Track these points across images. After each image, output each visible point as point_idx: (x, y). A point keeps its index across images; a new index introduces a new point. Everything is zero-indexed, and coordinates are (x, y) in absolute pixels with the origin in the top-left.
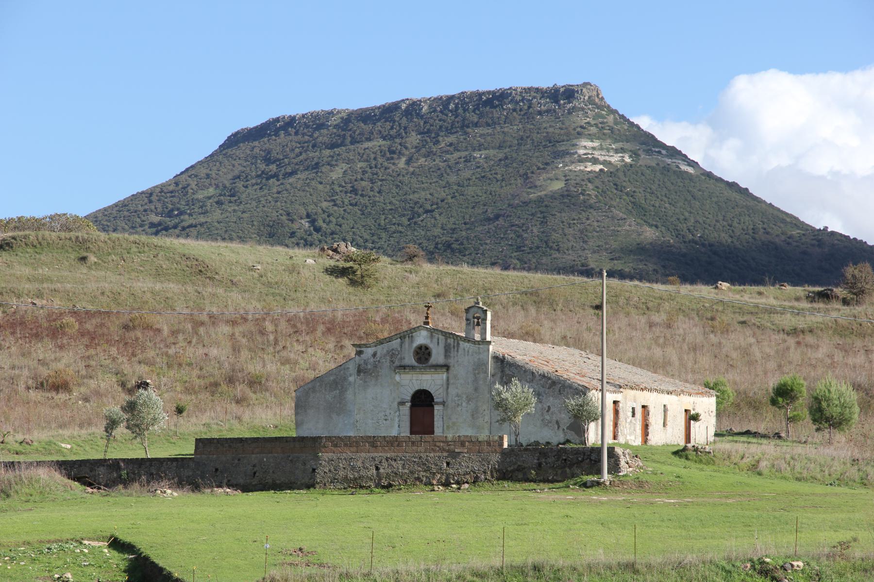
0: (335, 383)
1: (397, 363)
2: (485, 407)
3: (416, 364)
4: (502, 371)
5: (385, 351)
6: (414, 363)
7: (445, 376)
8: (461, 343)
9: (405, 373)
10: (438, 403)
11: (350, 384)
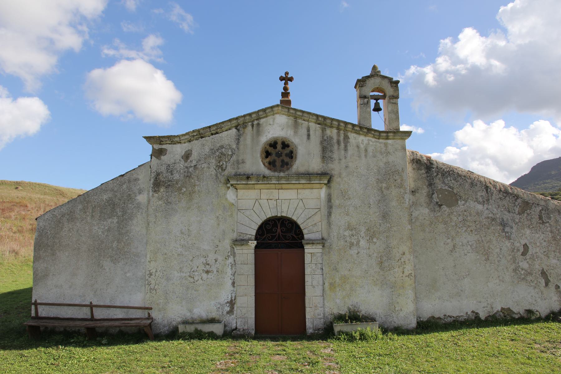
0: (112, 205)
1: (230, 170)
2: (404, 248)
3: (267, 172)
4: (430, 185)
5: (207, 149)
6: (263, 170)
7: (323, 192)
8: (352, 136)
9: (247, 187)
10: (312, 242)
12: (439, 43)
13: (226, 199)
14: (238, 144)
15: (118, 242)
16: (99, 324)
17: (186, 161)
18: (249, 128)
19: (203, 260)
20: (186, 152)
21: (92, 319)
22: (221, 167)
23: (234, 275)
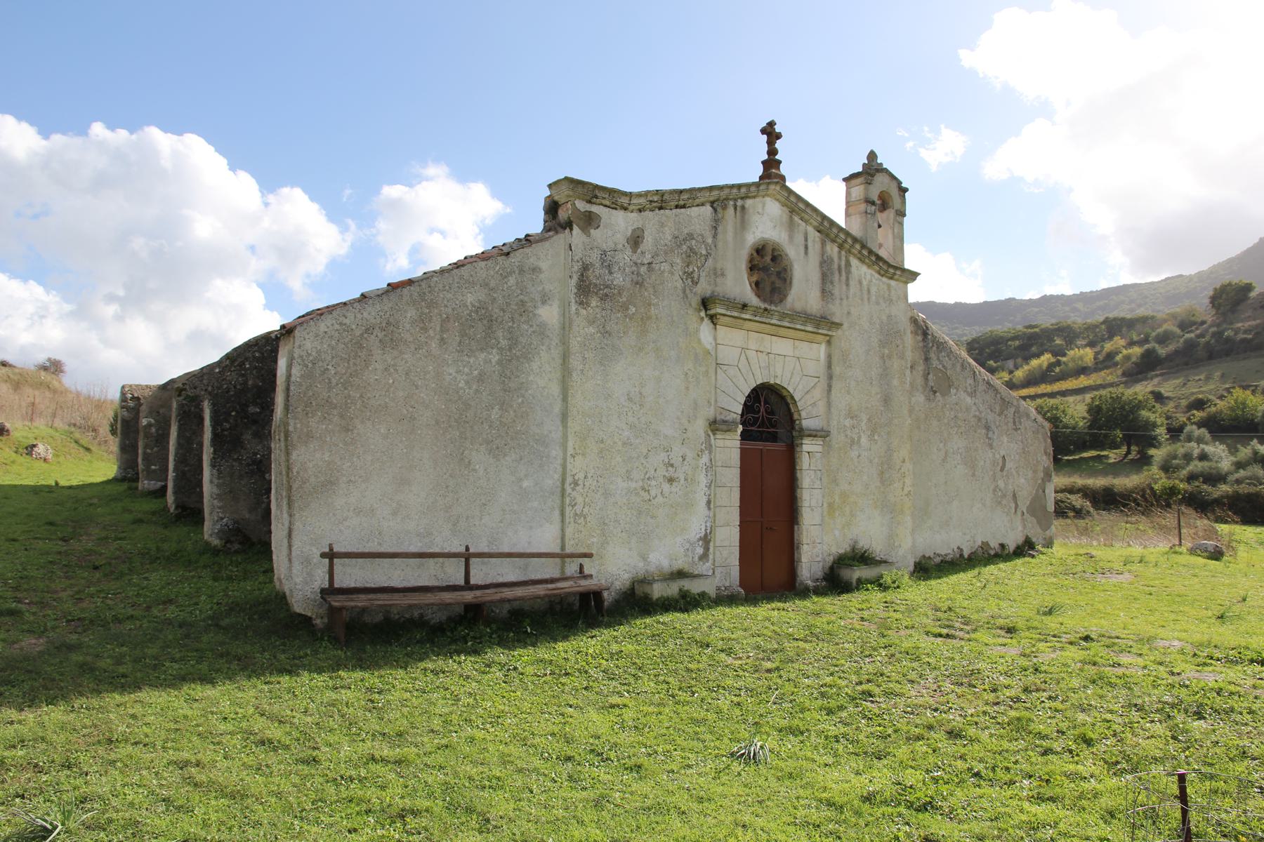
3: (754, 300)
4: (927, 359)
5: (668, 237)
11: (542, 331)
12: (377, 192)
13: (699, 340)
14: (715, 236)
15: (501, 409)
16: (490, 595)
17: (635, 252)
18: (731, 210)
19: (663, 456)
20: (634, 231)
21: (468, 586)
22: (689, 275)
23: (709, 487)
